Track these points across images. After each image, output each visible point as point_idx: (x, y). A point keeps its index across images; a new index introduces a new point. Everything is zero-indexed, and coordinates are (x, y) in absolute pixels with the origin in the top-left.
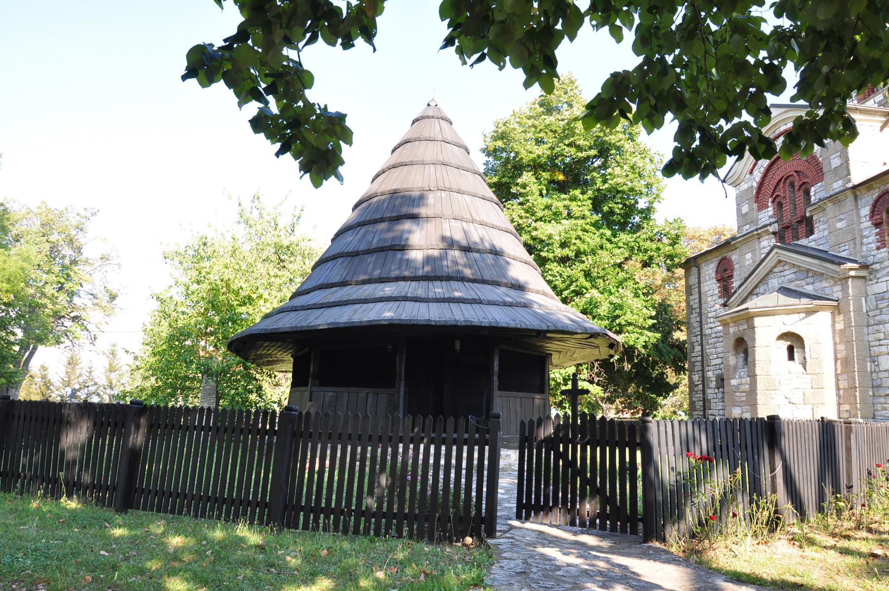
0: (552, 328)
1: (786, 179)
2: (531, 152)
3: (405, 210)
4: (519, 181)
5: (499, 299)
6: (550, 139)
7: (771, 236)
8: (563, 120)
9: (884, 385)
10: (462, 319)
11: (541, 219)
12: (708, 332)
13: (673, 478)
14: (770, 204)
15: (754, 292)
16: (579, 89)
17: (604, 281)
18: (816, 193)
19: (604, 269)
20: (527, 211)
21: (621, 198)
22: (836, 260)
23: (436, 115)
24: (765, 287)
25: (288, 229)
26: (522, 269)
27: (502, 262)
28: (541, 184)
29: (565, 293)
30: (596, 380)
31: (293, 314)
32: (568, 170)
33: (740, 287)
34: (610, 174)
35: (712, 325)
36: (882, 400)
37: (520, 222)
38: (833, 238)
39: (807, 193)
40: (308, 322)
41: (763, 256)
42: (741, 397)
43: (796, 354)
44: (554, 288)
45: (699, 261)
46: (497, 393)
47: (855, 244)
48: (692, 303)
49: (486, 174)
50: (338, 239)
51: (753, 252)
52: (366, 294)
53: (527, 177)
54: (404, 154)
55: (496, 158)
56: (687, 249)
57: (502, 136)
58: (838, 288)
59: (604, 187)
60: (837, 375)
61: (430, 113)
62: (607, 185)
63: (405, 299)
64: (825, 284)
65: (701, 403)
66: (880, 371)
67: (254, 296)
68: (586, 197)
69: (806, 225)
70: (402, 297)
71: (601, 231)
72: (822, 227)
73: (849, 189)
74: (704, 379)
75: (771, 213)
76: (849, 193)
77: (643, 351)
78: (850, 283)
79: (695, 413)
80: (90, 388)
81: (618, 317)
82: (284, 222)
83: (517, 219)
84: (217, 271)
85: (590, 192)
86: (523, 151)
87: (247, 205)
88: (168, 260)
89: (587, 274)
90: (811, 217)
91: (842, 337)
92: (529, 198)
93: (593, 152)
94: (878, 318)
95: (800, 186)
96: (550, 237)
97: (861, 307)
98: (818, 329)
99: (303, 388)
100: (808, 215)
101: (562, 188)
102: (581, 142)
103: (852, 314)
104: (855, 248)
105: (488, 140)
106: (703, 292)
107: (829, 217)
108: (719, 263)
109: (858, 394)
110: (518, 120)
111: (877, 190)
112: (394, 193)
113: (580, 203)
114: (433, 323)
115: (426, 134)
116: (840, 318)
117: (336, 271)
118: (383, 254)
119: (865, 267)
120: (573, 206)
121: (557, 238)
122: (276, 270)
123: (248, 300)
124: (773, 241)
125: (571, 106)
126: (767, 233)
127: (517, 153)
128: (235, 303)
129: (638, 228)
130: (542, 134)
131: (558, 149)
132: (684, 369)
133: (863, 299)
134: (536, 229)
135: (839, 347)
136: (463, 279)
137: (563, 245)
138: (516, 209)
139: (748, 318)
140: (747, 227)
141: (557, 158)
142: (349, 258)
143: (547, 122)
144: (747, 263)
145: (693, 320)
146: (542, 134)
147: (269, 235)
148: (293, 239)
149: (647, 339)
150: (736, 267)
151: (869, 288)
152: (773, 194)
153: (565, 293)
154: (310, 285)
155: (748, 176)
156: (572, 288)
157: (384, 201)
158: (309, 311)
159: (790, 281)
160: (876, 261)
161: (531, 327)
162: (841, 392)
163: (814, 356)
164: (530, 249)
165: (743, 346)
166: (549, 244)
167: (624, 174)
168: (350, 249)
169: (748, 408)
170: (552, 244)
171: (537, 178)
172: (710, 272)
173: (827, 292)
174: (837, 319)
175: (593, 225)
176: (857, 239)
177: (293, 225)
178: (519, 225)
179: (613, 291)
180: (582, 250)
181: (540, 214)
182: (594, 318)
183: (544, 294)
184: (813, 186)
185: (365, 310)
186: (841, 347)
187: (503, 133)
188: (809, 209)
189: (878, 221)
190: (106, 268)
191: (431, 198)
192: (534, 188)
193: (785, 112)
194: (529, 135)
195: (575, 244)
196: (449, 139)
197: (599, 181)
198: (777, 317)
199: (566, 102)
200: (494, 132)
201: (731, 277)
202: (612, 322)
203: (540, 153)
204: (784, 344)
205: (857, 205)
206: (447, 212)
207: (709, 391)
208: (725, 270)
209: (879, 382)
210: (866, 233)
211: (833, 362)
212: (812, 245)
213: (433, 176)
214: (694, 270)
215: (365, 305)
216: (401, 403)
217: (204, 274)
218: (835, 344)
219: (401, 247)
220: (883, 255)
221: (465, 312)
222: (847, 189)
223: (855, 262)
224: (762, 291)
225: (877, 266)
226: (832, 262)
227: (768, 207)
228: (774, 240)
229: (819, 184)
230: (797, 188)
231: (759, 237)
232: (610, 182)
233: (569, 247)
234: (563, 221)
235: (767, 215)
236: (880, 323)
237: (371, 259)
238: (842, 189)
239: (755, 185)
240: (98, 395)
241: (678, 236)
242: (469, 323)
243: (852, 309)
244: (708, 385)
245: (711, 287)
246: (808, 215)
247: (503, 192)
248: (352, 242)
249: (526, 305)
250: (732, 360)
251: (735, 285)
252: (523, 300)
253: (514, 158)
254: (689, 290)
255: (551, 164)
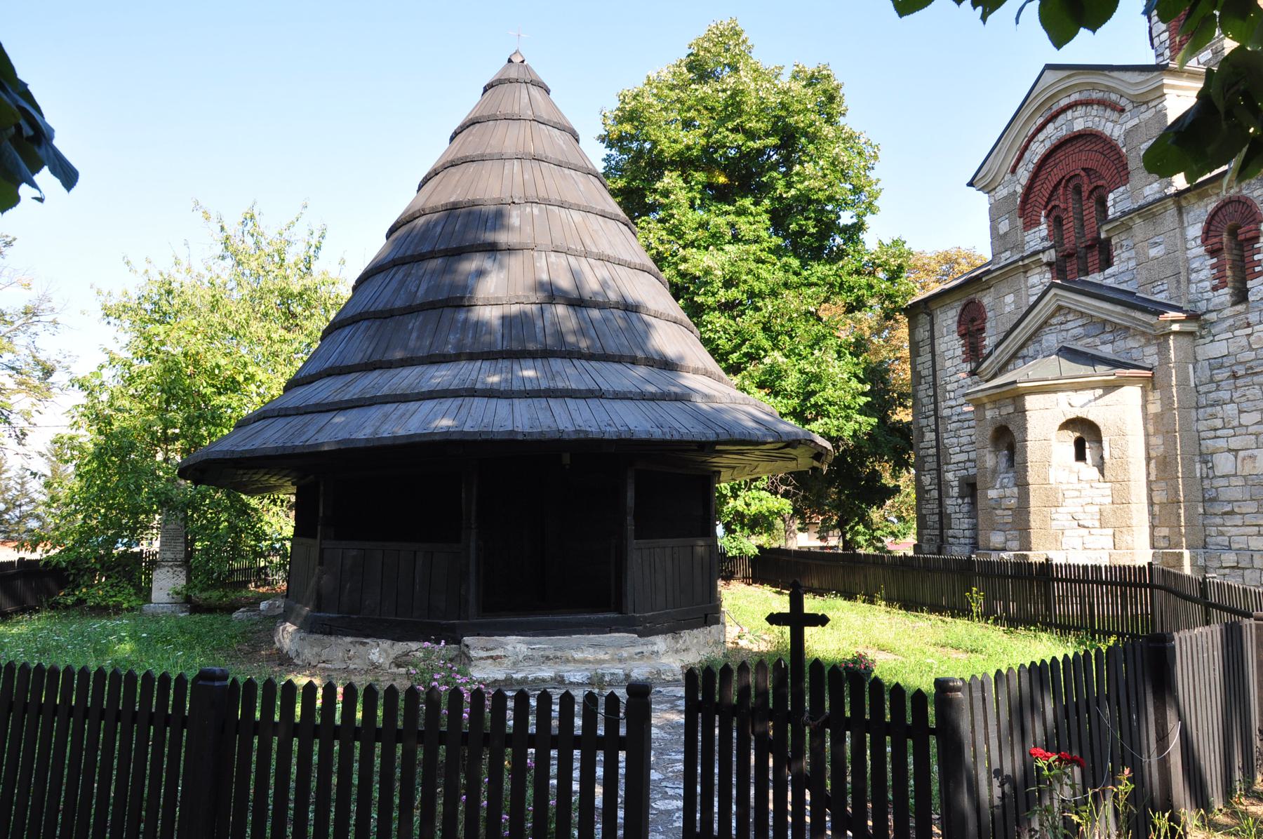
0: (724, 437)
1: (1068, 181)
2: (675, 141)
3: (470, 238)
4: (659, 185)
5: (634, 389)
6: (704, 121)
7: (1044, 268)
8: (724, 91)
9: (1222, 498)
10: (571, 428)
11: (692, 244)
12: (946, 412)
13: (997, 792)
14: (1042, 219)
15: (1020, 354)
16: (749, 43)
17: (791, 338)
18: (1115, 203)
19: (790, 320)
20: (671, 232)
21: (815, 211)
22: (1150, 306)
23: (522, 77)
24: (1037, 346)
25: (301, 266)
26: (672, 337)
27: (639, 326)
28: (691, 189)
29: (734, 357)
30: (782, 489)
31: (281, 422)
32: (730, 167)
33: (997, 346)
34: (798, 174)
35: (953, 403)
36: (1218, 520)
37: (661, 249)
38: (1144, 272)
39: (1102, 203)
40: (304, 438)
41: (1034, 299)
42: (1004, 516)
43: (1087, 451)
44: (715, 352)
45: (932, 306)
46: (633, 543)
47: (1178, 282)
48: (919, 368)
49: (606, 175)
50: (362, 288)
51: (1017, 292)
52: (404, 385)
53: (670, 179)
54: (472, 143)
55: (622, 150)
56: (918, 288)
57: (632, 116)
58: (1152, 350)
59: (789, 195)
60: (1149, 483)
61: (513, 74)
62: (793, 192)
63: (472, 393)
64: (1131, 343)
65: (936, 518)
66: (1215, 477)
67: (240, 378)
68: (760, 209)
69: (1100, 253)
70: (466, 390)
71: (784, 259)
72: (1125, 255)
73: (1171, 196)
74: (941, 484)
75: (1045, 233)
76: (1170, 202)
77: (851, 443)
78: (1171, 342)
79: (925, 532)
80: (24, 508)
81: (813, 393)
82: (294, 254)
83: (655, 244)
84: (178, 340)
85: (767, 202)
86: (664, 140)
87: (233, 228)
88: (111, 319)
89: (766, 328)
90: (1108, 240)
91: (1157, 425)
92: (675, 211)
93: (773, 141)
94: (1212, 396)
95: (1091, 192)
96: (707, 272)
97: (1187, 379)
98: (1123, 412)
99: (310, 541)
100: (1103, 236)
101: (722, 195)
102: (752, 125)
103: (1174, 390)
104: (1178, 288)
105: (609, 122)
106: (938, 352)
107: (1137, 240)
108: (963, 310)
109: (1182, 511)
110: (655, 91)
111: (1214, 198)
112: (452, 208)
113: (754, 220)
114: (520, 437)
115: (506, 108)
116: (1155, 396)
117: (356, 346)
118: (434, 314)
119: (1193, 317)
120: (742, 222)
121: (719, 273)
122: (283, 332)
123: (232, 386)
124: (1048, 277)
125: (735, 69)
126: (1039, 263)
127: (655, 143)
128: (209, 390)
129: (841, 254)
130: (692, 114)
131: (717, 136)
132: (906, 465)
133: (1191, 366)
134: (685, 260)
135: (1153, 440)
136: (572, 354)
137: (728, 284)
138: (652, 228)
139: (1015, 397)
140: (1008, 254)
141: (716, 151)
142: (378, 323)
143: (700, 94)
144: (1007, 309)
145: (921, 394)
146: (692, 114)
147: (272, 275)
148: (308, 282)
149: (857, 426)
150: (989, 314)
151: (1199, 350)
152: (1047, 203)
153: (734, 357)
154: (312, 370)
155: (1008, 176)
156: (744, 349)
157: (436, 223)
158: (308, 417)
159: (1077, 338)
160: (1211, 308)
161: (690, 438)
162: (1156, 508)
163: (1116, 453)
164: (677, 292)
165: (1008, 440)
166: (706, 283)
167: (820, 174)
168: (379, 306)
169: (1016, 533)
170: (711, 283)
171: (685, 181)
172: (950, 322)
173: (1135, 356)
174: (1151, 398)
175: (770, 251)
176: (1181, 274)
177: (308, 262)
178: (658, 253)
179: (804, 354)
180: (757, 291)
181: (691, 236)
182: (776, 395)
183: (707, 373)
184: (1111, 191)
185: (401, 417)
186: (1156, 441)
187: (632, 111)
188: (1106, 228)
189: (1216, 246)
190: (33, 329)
191: (515, 218)
192: (682, 196)
193: (1069, 77)
194: (673, 115)
195: (745, 282)
196: (545, 117)
197: (780, 185)
198: (1060, 395)
199: (729, 65)
200: (618, 109)
201: (983, 330)
202: (804, 400)
203: (691, 143)
204: (1070, 436)
205: (1181, 221)
206: (543, 240)
207: (949, 502)
208: (973, 320)
209: (1213, 493)
210: (1195, 265)
211: (1144, 463)
212: (1110, 282)
213: (518, 179)
214: (923, 319)
215: (403, 407)
216: (472, 568)
217: (156, 345)
218: (1147, 435)
219: (459, 300)
220: (1223, 299)
221: (575, 415)
222: (1167, 197)
223: (1179, 309)
224: (1031, 352)
225: (1213, 317)
226: (1144, 310)
227: (1040, 224)
228: (1048, 275)
229: (1121, 189)
230: (1085, 194)
231: (1026, 269)
232: (799, 186)
233: (737, 286)
234: (727, 247)
235: (1038, 237)
236: (1216, 403)
237: (414, 323)
238: (1158, 196)
239: (1019, 190)
240: (38, 517)
241: (900, 267)
242: (582, 436)
243: (1174, 383)
244: (947, 492)
245: (950, 345)
246: (1103, 236)
247: (635, 202)
248: (386, 294)
249: (682, 397)
250: (990, 460)
251: (989, 341)
252: (674, 389)
253: (650, 150)
254: (915, 347)
255: (704, 159)
